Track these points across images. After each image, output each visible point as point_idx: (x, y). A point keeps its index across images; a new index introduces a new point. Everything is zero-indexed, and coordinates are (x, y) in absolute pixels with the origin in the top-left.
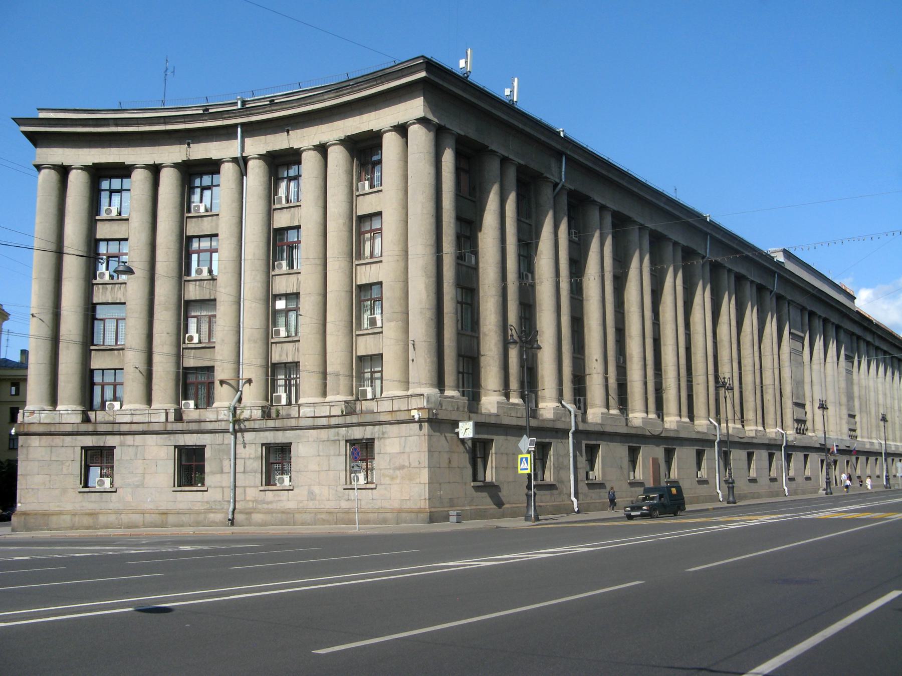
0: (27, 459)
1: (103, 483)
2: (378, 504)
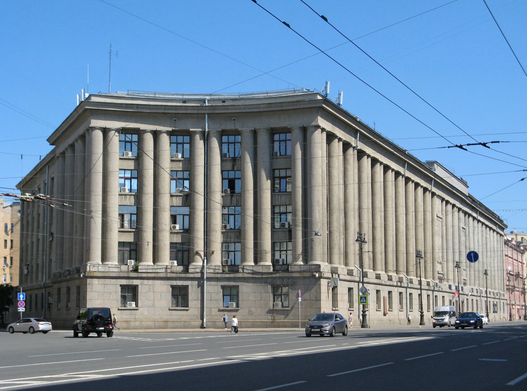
0: (92, 291)
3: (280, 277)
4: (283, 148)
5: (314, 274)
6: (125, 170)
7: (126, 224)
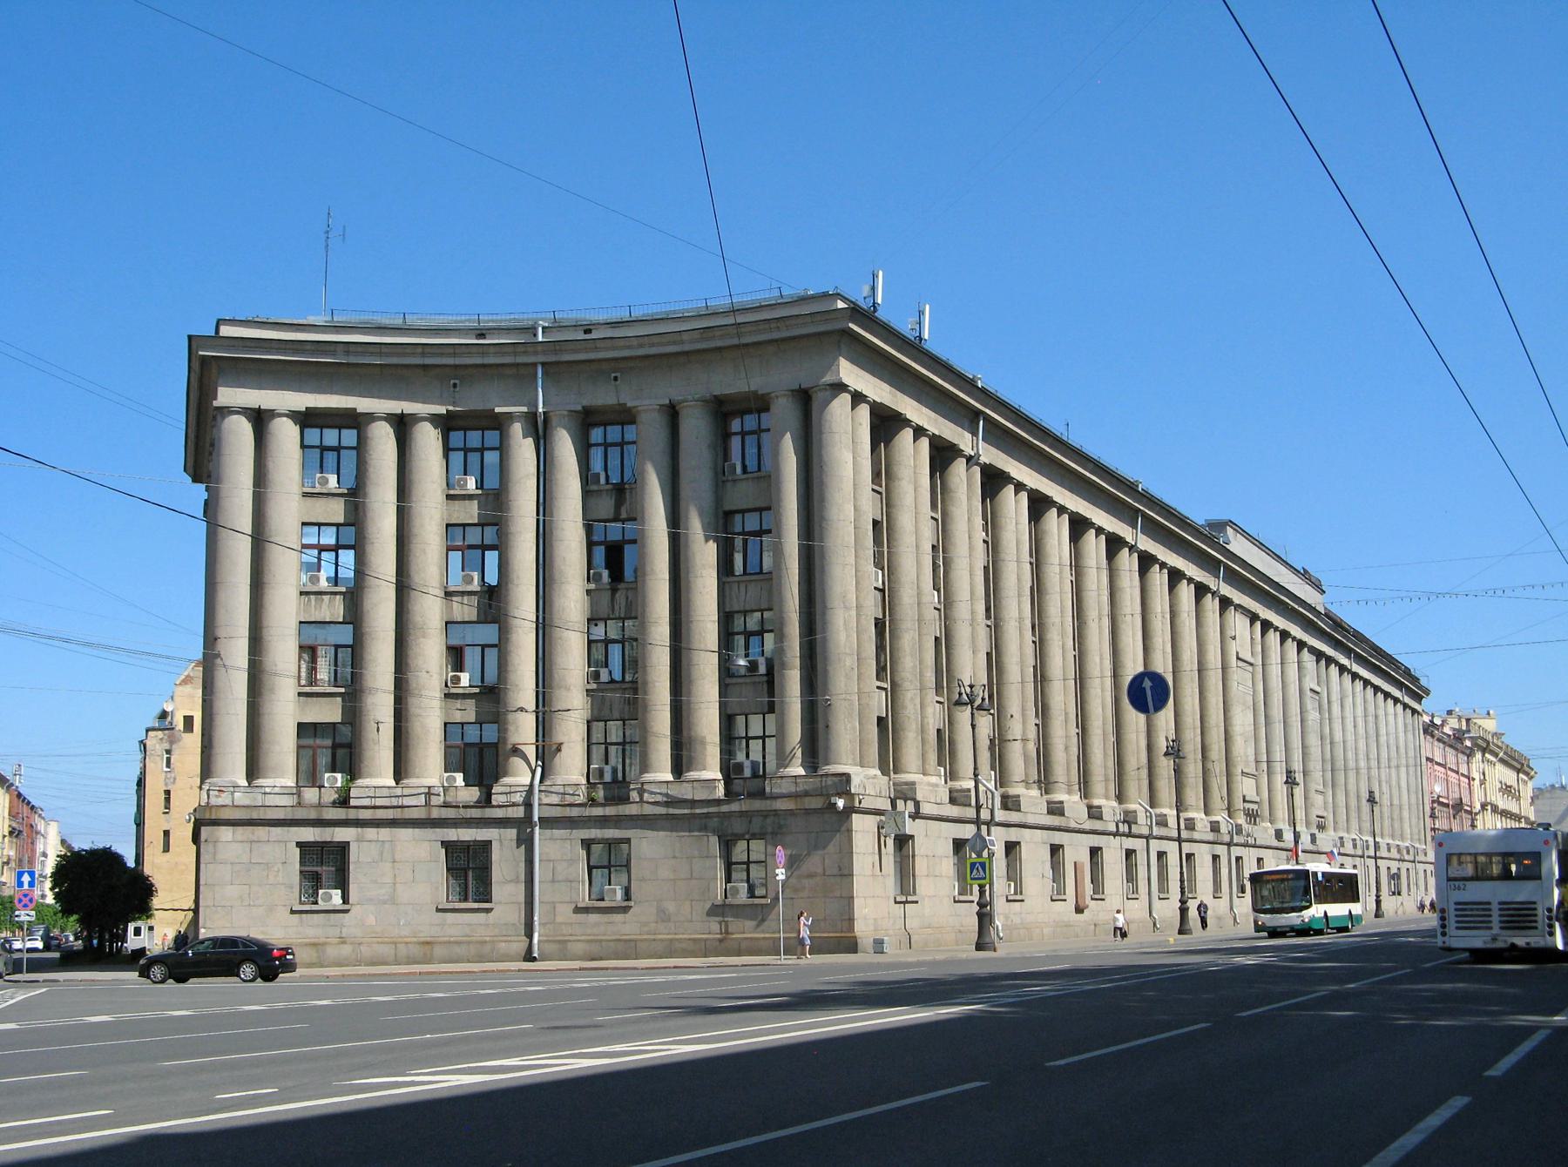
0: (214, 861)
3: (742, 814)
4: (751, 451)
5: (833, 800)
6: (319, 525)
7: (323, 674)
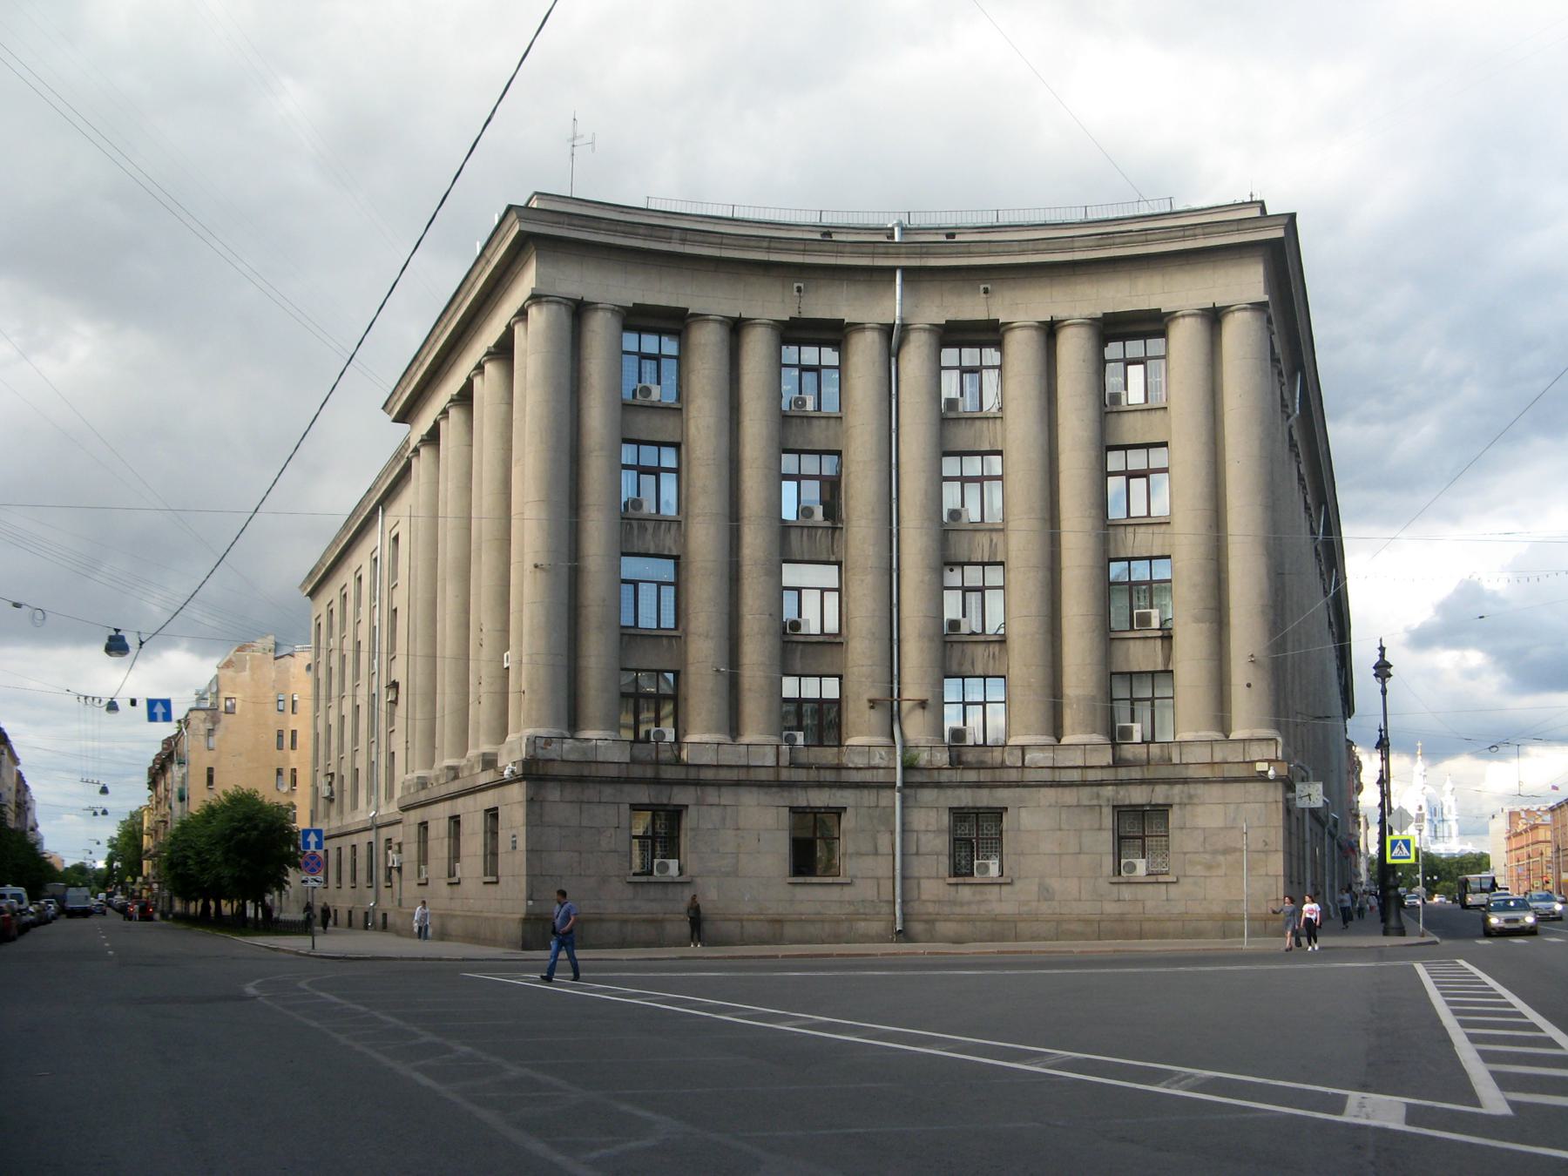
1: (667, 867)
2: (1178, 908)
